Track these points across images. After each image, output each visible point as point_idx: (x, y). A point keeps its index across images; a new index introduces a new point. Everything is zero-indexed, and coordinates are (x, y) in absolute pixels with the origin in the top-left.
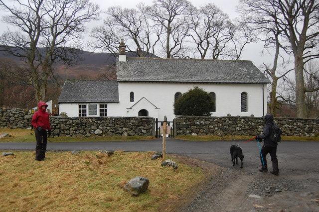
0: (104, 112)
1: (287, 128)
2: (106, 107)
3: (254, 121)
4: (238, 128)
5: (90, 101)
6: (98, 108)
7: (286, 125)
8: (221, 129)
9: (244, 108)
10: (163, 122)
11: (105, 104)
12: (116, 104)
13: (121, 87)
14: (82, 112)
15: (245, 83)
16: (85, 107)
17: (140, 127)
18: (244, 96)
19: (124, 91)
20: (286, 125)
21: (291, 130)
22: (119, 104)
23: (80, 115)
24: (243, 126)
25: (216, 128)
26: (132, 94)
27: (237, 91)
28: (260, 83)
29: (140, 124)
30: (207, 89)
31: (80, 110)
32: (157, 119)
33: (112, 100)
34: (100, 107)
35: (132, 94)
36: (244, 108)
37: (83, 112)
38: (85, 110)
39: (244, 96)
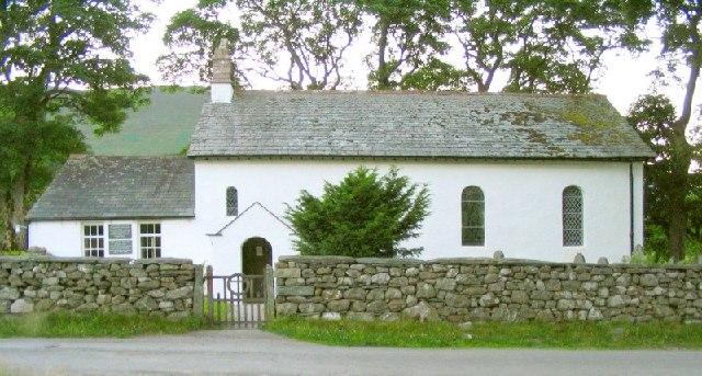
0: (151, 248)
1: (660, 299)
2: (158, 231)
3: (543, 275)
4: (487, 297)
5: (115, 215)
6: (136, 236)
7: (659, 290)
8: (428, 300)
9: (572, 234)
10: (230, 278)
11: (154, 222)
12: (578, 205)
13: (202, 172)
14: (93, 245)
15: (524, 159)
16: (101, 232)
17: (154, 293)
18: (572, 197)
19: (210, 182)
20: (659, 290)
21: (674, 307)
22: (193, 221)
23: (88, 253)
24: (505, 292)
25: (410, 299)
26: (232, 195)
27: (547, 185)
28: (619, 159)
29: (155, 283)
30: (381, 173)
31: (87, 241)
32: (210, 269)
33: (47, 215)
34: (143, 231)
35: (232, 195)
36: (572, 234)
37: (94, 245)
38: (101, 241)
39: (572, 197)
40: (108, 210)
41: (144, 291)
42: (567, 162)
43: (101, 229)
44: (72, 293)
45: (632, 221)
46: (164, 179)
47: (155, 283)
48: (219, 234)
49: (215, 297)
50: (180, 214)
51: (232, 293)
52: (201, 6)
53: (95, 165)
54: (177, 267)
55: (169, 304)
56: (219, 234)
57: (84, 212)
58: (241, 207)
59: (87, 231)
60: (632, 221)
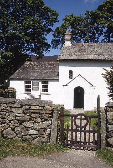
38: (30, 86)
40: (33, 77)
41: (21, 122)
42: (54, 81)
43: (30, 82)
44: (9, 109)
45: (83, 78)
46: (50, 68)
47: (27, 117)
48: (66, 85)
49: (65, 127)
50: (54, 78)
51: (77, 126)
52: (35, 1)
53: (32, 64)
54: (41, 108)
55: (35, 132)
56: (66, 85)
57: (25, 77)
58: (74, 77)
59: (26, 83)
60: (83, 78)
